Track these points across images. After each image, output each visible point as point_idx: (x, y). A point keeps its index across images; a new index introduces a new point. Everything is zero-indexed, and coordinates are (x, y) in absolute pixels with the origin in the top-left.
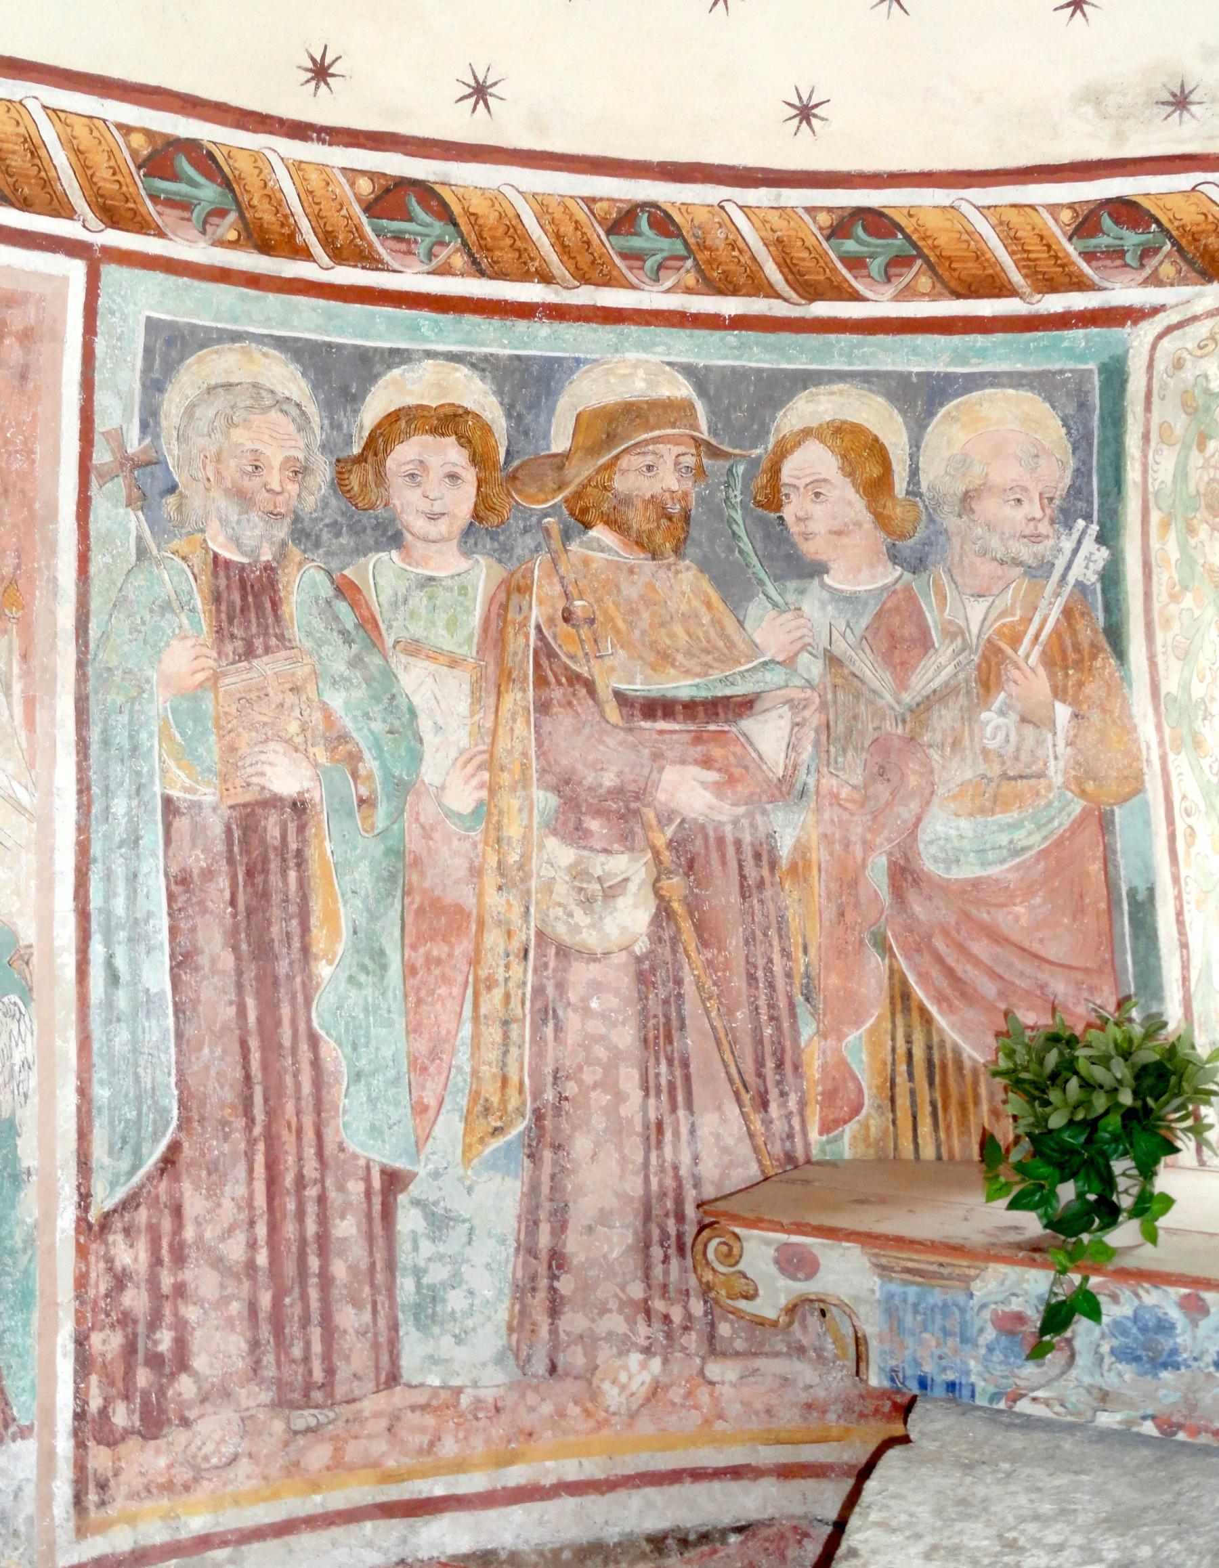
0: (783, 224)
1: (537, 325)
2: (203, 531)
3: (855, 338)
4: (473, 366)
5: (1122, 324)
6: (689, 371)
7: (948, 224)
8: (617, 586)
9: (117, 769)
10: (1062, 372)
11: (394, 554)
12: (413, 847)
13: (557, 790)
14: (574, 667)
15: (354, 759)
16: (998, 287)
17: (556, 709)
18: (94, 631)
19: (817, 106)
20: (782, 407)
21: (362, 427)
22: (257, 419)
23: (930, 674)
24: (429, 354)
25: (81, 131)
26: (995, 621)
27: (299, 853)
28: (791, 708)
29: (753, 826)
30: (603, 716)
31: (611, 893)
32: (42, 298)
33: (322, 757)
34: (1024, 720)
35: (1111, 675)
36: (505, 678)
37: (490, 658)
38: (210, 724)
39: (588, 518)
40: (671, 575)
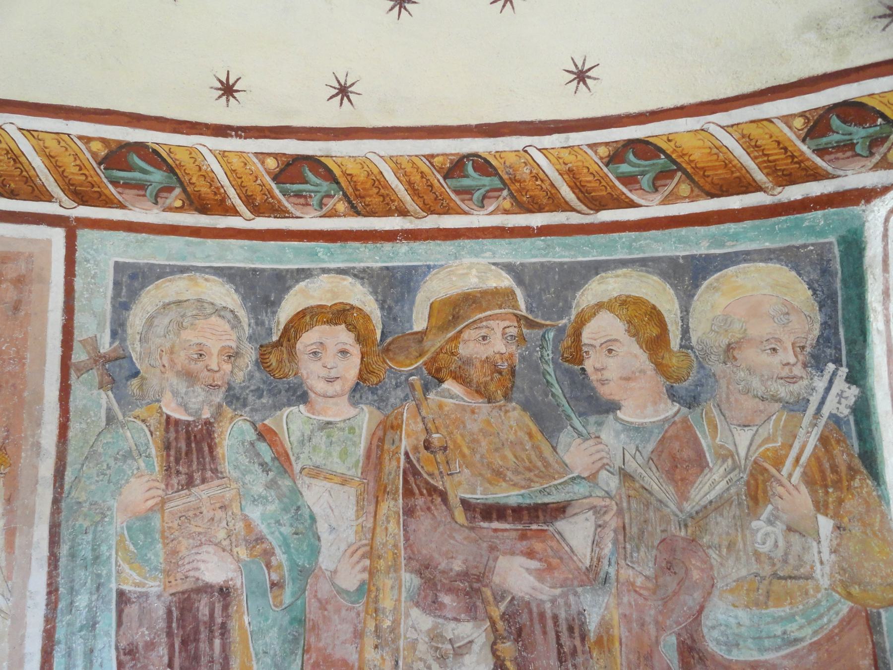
0: (572, 158)
1: (399, 245)
2: (159, 401)
3: (633, 235)
4: (355, 276)
5: (857, 203)
6: (509, 268)
7: (700, 143)
8: (463, 423)
9: (81, 574)
10: (805, 246)
11: (302, 407)
12: (312, 617)
13: (420, 573)
14: (432, 482)
15: (268, 554)
16: (747, 186)
17: (419, 513)
18: (69, 476)
19: (589, 70)
20: (580, 288)
21: (278, 323)
22: (201, 323)
23: (706, 488)
24: (325, 271)
25: (51, 143)
26: (760, 446)
27: (223, 626)
28: (595, 513)
29: (568, 605)
30: (453, 518)
31: (459, 652)
32: (31, 256)
33: (243, 553)
34: (790, 529)
35: (869, 494)
36: (381, 492)
37: (371, 477)
38: (157, 536)
39: (442, 375)
40: (502, 414)
